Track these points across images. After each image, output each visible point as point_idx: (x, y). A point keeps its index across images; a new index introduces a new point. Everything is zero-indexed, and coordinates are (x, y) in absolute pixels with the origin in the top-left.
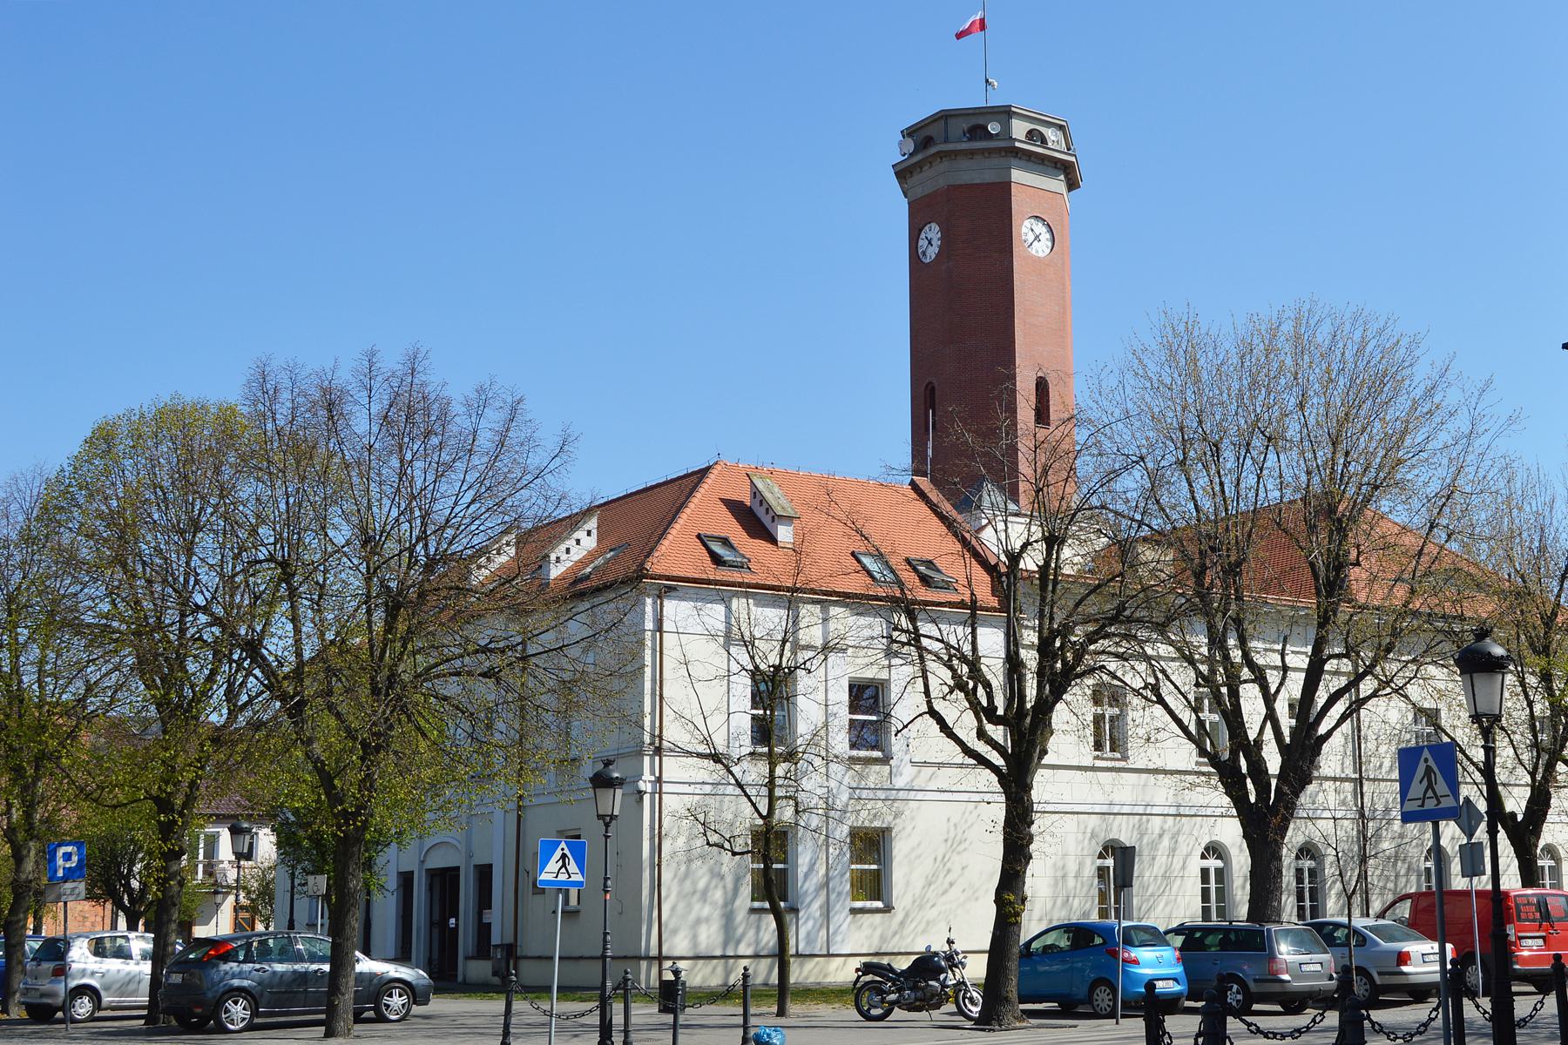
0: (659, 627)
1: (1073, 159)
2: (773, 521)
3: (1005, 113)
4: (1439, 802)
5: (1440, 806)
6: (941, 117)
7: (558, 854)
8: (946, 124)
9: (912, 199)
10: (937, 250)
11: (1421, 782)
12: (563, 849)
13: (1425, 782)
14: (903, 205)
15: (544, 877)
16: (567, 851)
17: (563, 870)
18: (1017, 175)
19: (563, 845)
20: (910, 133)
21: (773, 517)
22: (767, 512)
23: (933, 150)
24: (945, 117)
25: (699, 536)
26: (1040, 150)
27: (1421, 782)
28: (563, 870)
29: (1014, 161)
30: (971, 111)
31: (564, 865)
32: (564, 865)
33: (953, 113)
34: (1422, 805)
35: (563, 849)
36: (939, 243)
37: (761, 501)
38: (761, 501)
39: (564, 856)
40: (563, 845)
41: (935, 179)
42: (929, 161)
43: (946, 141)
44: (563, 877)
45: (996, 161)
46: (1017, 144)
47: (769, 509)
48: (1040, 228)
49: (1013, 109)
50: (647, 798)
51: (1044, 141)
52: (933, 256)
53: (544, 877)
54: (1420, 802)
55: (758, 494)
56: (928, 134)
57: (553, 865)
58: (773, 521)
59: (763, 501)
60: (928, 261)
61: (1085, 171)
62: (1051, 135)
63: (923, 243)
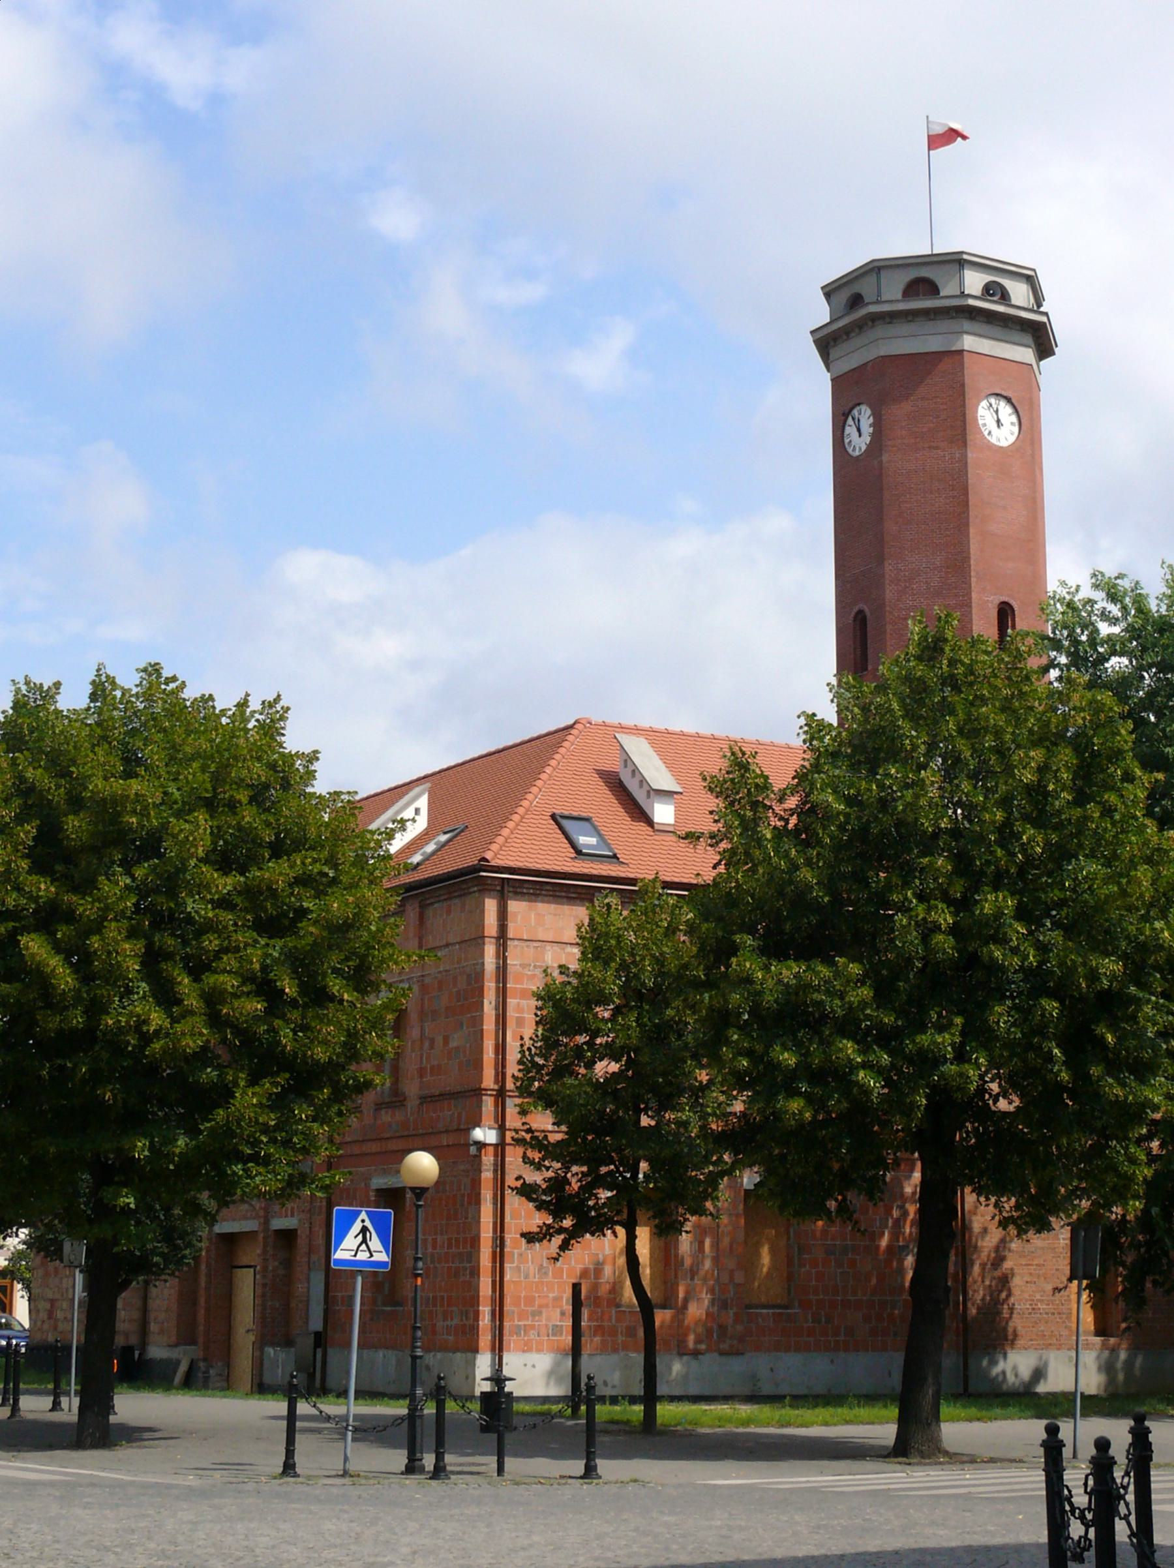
0: (502, 937)
1: (1044, 319)
2: (649, 796)
3: (957, 262)
4: (371, 1256)
5: (372, 1259)
6: (872, 270)
7: (357, 1227)
8: (879, 279)
9: (835, 376)
10: (868, 440)
11: (356, 1237)
12: (363, 1221)
13: (360, 1238)
14: (827, 377)
15: (339, 1255)
16: (368, 1224)
17: (364, 1247)
18: (969, 342)
19: (363, 1215)
20: (830, 291)
21: (648, 792)
22: (641, 786)
23: (862, 312)
24: (876, 269)
25: (553, 817)
26: (1000, 308)
27: (356, 1237)
28: (364, 1247)
29: (967, 325)
30: (900, 262)
31: (364, 1241)
32: (364, 1241)
33: (888, 263)
34: (355, 1256)
35: (363, 1221)
36: (871, 430)
37: (634, 771)
38: (634, 771)
39: (364, 1230)
40: (363, 1215)
41: (853, 357)
42: (860, 326)
43: (878, 302)
44: (363, 1256)
45: (944, 325)
46: (971, 302)
47: (643, 781)
48: (1005, 410)
49: (965, 257)
50: (488, 1159)
51: (1004, 297)
52: (864, 448)
53: (339, 1255)
54: (353, 1253)
55: (629, 762)
56: (856, 291)
57: (351, 1241)
58: (649, 796)
59: (635, 771)
60: (857, 453)
61: (1060, 329)
62: (1011, 285)
63: (850, 430)
